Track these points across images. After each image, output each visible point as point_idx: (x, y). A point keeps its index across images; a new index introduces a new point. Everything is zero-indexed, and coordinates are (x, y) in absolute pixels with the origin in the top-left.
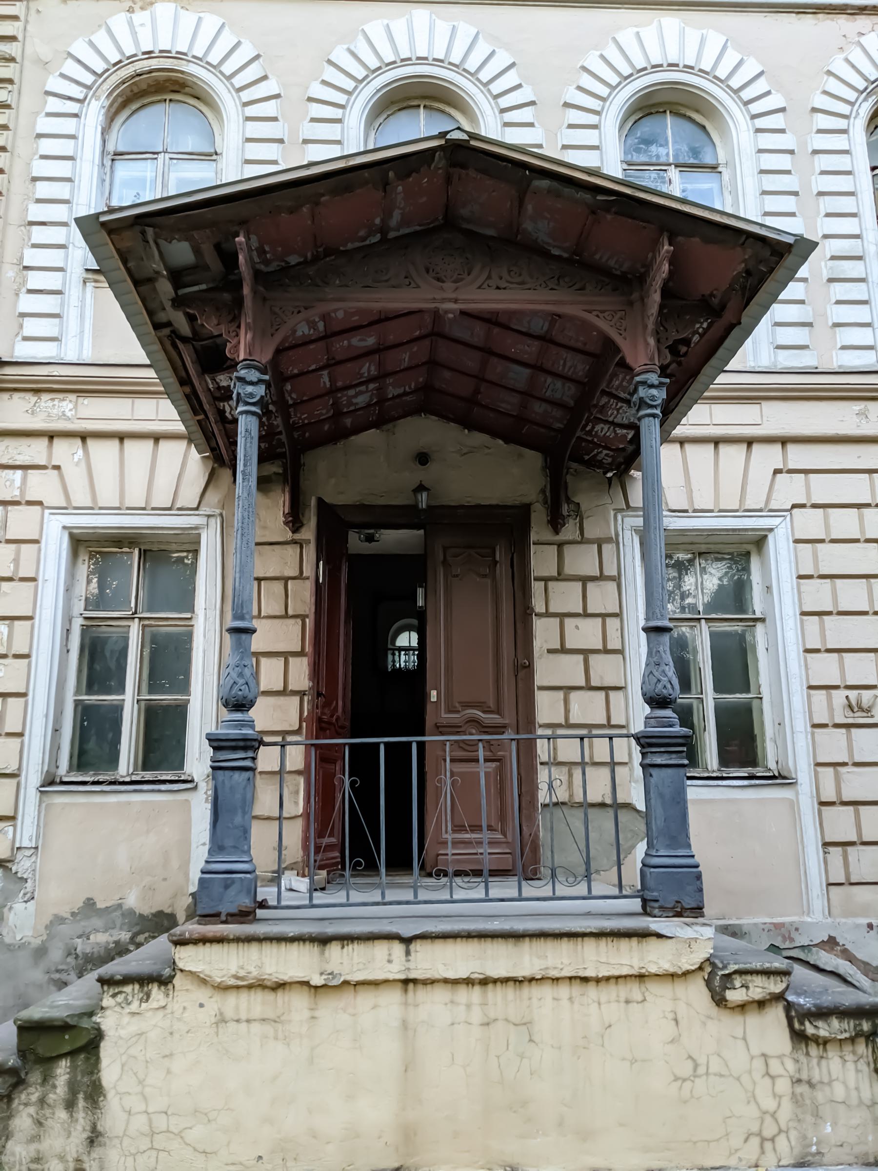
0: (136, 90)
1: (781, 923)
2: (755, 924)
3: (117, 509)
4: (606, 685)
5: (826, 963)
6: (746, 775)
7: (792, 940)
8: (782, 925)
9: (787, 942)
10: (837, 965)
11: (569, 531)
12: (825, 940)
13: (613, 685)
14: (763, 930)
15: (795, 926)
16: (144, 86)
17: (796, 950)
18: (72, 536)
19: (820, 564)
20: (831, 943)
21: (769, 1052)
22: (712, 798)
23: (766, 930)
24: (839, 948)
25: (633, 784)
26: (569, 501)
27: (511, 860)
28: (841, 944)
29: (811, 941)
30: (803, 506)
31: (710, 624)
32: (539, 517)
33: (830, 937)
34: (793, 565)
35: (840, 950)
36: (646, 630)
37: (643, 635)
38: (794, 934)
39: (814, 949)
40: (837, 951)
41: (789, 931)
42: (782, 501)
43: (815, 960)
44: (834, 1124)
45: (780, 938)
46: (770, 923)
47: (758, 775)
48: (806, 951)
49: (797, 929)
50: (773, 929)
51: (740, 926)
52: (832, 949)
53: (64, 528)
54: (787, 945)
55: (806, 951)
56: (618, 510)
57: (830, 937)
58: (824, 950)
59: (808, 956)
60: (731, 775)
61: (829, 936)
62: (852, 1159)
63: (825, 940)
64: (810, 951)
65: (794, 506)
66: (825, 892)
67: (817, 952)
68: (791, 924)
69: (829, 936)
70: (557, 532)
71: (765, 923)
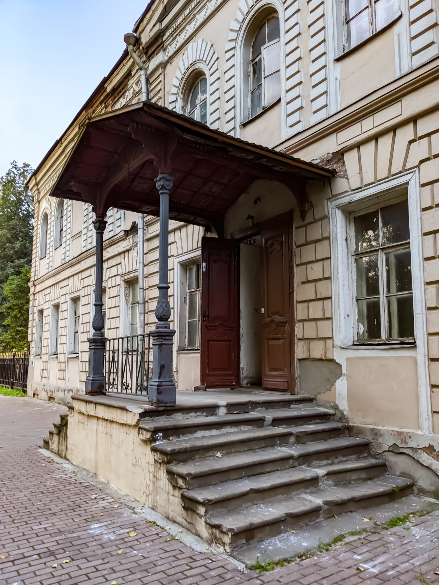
0: (190, 84)
1: (401, 432)
2: (388, 431)
3: (188, 252)
4: (323, 297)
5: (424, 461)
6: (399, 342)
7: (406, 443)
8: (402, 433)
9: (403, 444)
10: (432, 463)
11: (309, 218)
12: (427, 447)
13: (325, 297)
14: (392, 434)
15: (409, 435)
16: (192, 81)
17: (409, 450)
18: (181, 264)
19: (435, 197)
20: (430, 449)
21: (150, 463)
22: (371, 356)
23: (393, 435)
24: (435, 453)
25: (334, 349)
26: (308, 202)
27: (286, 385)
28: (437, 451)
29: (418, 446)
30: (428, 159)
31: (385, 251)
32: (297, 215)
33: (430, 445)
34: (419, 203)
35: (436, 455)
36: (95, 305)
37: (94, 307)
38: (408, 440)
39: (420, 451)
40: (434, 454)
41: (406, 438)
42: (412, 162)
43: (418, 458)
44: (160, 497)
45: (400, 441)
46: (396, 431)
47: (405, 342)
48: (414, 451)
49: (410, 437)
50: (397, 435)
51: (380, 430)
52: (431, 453)
53: (178, 262)
54: (403, 445)
55: (414, 451)
56: (329, 199)
57: (430, 445)
58: (426, 453)
59: (414, 454)
60: (391, 342)
61: (429, 444)
62: (163, 513)
63: (427, 447)
64: (416, 451)
65: (422, 162)
66: (431, 418)
67: (421, 454)
68: (407, 433)
69: (429, 444)
70: (304, 219)
71: (393, 431)
